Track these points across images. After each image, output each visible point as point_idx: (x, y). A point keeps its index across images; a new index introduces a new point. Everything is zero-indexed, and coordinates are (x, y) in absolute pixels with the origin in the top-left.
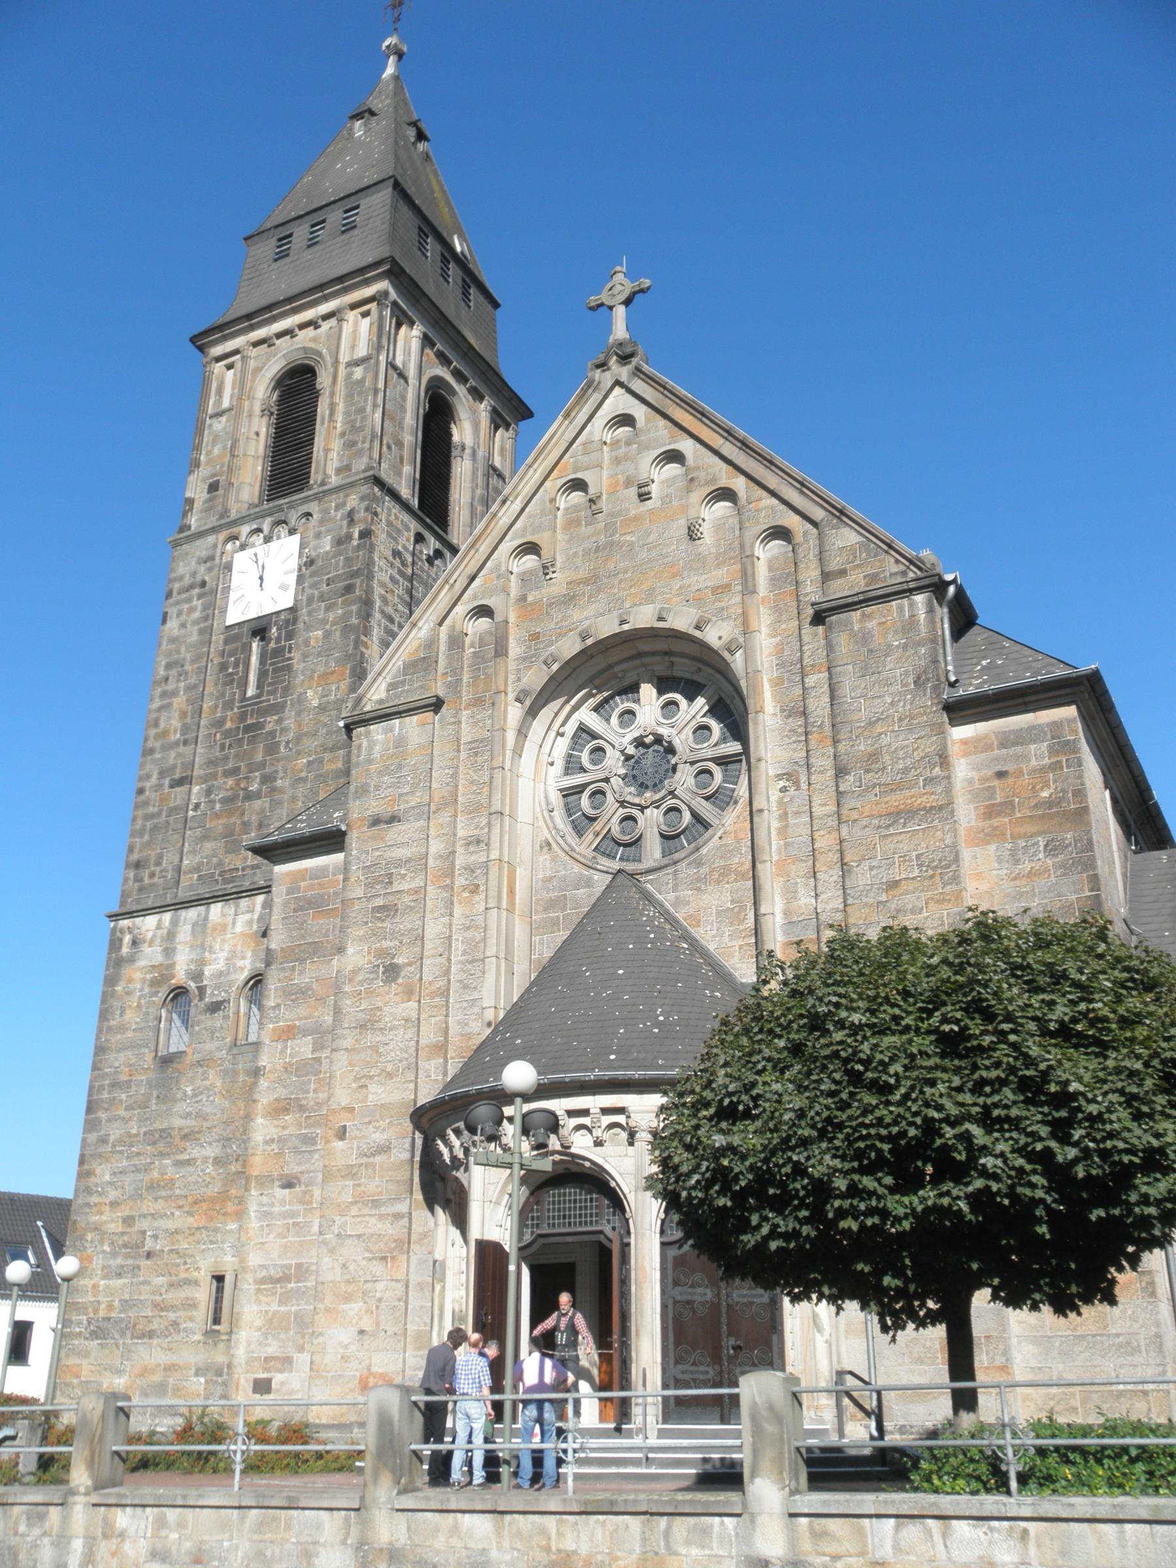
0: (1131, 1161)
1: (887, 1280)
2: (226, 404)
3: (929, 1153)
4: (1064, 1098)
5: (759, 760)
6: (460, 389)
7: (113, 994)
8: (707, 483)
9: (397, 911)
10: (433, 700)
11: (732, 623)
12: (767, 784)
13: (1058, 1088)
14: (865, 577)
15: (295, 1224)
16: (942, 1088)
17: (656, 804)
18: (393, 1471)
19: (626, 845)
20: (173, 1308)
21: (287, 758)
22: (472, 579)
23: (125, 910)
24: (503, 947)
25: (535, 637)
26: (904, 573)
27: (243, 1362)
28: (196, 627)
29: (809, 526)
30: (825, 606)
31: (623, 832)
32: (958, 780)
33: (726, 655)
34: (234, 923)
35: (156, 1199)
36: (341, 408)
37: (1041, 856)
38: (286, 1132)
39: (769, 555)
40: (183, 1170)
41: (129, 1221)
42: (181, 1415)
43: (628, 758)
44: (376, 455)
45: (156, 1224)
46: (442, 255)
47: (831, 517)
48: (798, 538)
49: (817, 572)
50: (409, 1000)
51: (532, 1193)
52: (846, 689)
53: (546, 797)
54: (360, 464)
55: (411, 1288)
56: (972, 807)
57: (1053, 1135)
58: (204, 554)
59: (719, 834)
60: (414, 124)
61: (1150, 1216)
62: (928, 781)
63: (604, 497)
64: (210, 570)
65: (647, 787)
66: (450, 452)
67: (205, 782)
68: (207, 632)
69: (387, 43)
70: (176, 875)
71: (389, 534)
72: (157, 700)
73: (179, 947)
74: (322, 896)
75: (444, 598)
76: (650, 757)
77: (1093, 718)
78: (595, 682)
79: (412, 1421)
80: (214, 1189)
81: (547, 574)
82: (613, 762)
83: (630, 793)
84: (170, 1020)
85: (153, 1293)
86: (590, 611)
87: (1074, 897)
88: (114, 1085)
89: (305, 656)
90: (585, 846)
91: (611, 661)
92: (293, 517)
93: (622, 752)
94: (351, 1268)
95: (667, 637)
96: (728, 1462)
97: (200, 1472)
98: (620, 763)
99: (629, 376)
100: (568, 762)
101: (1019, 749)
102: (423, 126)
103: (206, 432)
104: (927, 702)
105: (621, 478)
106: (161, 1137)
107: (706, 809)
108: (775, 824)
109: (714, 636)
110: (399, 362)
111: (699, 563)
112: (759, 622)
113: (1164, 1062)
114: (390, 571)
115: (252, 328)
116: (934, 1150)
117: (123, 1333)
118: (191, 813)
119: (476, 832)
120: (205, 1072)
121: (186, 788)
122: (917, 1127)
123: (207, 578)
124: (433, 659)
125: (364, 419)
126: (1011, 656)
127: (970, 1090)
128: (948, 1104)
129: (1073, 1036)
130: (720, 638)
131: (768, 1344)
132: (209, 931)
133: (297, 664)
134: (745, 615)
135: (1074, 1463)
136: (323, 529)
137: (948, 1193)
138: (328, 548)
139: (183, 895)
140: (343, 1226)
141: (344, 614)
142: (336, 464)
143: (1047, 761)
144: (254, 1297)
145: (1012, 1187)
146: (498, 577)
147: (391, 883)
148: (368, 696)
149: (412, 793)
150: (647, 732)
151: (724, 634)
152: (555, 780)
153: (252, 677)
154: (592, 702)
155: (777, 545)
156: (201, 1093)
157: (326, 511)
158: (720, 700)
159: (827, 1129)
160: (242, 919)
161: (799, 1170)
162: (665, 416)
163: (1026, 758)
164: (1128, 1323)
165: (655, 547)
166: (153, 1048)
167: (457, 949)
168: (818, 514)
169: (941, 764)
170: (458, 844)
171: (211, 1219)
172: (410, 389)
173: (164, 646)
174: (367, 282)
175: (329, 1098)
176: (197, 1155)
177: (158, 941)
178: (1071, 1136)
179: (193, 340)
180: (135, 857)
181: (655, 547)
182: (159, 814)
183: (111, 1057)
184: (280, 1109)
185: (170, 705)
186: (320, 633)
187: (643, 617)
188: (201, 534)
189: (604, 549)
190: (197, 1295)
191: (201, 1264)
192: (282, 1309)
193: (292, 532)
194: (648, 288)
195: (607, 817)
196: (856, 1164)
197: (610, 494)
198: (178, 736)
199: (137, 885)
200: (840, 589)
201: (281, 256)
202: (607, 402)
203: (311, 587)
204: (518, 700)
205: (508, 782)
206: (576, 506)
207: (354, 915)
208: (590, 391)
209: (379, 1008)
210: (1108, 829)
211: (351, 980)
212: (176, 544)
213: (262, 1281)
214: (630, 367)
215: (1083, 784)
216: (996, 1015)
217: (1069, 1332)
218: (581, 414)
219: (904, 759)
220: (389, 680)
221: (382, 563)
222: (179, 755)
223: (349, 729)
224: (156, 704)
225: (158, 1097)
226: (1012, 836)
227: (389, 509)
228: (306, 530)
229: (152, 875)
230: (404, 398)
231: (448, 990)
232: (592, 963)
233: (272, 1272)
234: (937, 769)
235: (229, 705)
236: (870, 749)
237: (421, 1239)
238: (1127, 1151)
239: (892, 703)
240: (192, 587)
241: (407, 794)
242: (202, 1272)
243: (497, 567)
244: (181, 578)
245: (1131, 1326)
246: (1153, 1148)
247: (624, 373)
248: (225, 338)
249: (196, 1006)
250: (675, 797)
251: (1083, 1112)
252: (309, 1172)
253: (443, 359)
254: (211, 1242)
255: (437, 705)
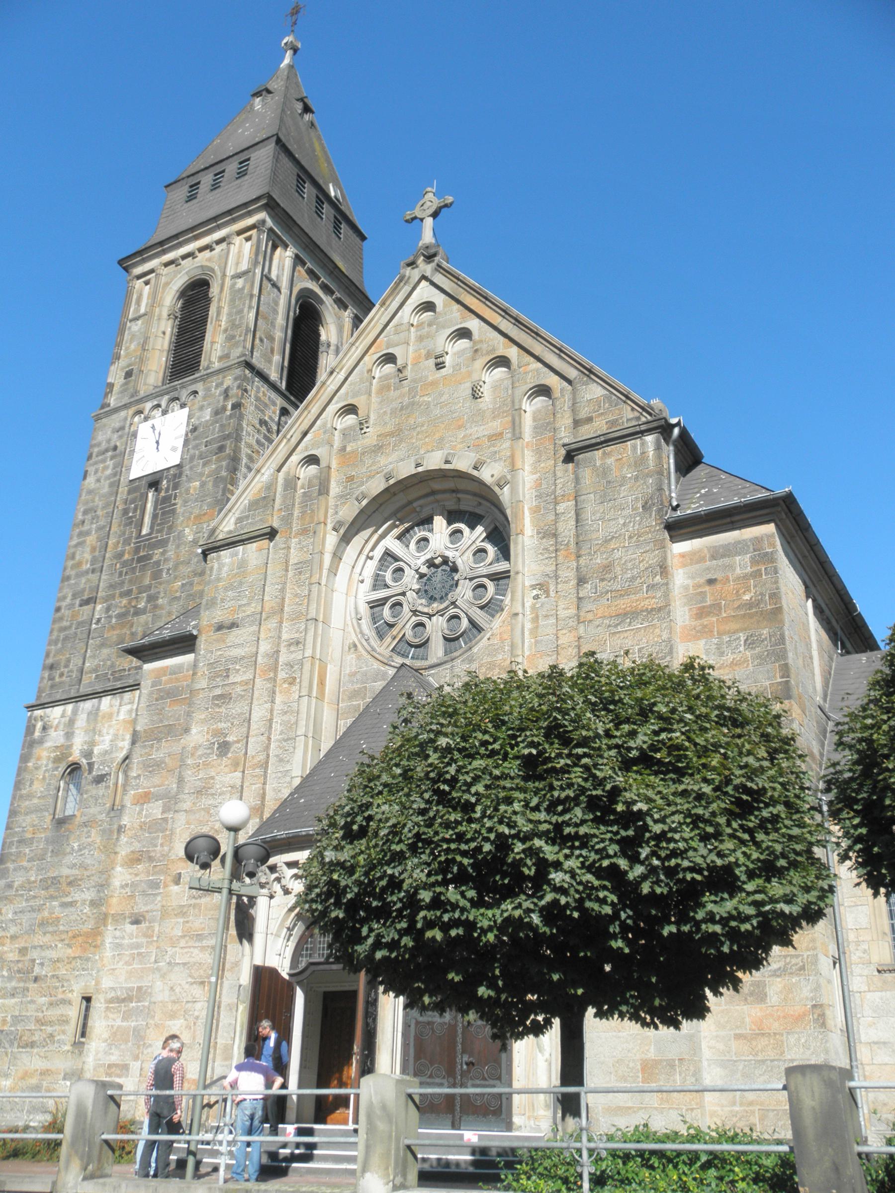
0: (693, 879)
1: (482, 991)
2: (142, 310)
3: (505, 868)
4: (631, 818)
5: (517, 573)
6: (328, 300)
7: (26, 769)
8: (488, 353)
9: (231, 698)
10: (268, 530)
11: (502, 463)
12: (523, 593)
13: (624, 808)
14: (607, 423)
15: (139, 954)
16: (517, 806)
17: (441, 613)
18: (81, 1159)
19: (417, 647)
20: (51, 1023)
21: (168, 582)
22: (305, 434)
23: (39, 702)
24: (311, 728)
25: (351, 479)
26: (638, 418)
27: (92, 1068)
28: (108, 482)
29: (565, 384)
30: (573, 446)
31: (415, 636)
32: (676, 587)
33: (496, 489)
34: (118, 712)
35: (45, 934)
36: (225, 310)
37: (742, 649)
38: (138, 878)
39: (533, 408)
40: (67, 910)
41: (23, 951)
42: (50, 1113)
43: (422, 576)
44: (249, 345)
45: (43, 954)
46: (317, 197)
47: (582, 376)
48: (556, 394)
49: (570, 421)
50: (235, 771)
51: (308, 928)
52: (588, 515)
53: (356, 608)
54: (236, 352)
55: (222, 1008)
56: (686, 608)
57: (624, 854)
58: (117, 425)
59: (488, 636)
60: (302, 100)
61: (715, 934)
62: (651, 587)
63: (409, 367)
64: (121, 437)
65: (435, 599)
66: (317, 348)
67: (106, 601)
68: (116, 485)
69: (285, 41)
70: (79, 674)
71: (257, 407)
72: (75, 538)
73: (77, 731)
74: (177, 688)
75: (283, 449)
76: (439, 575)
77: (792, 537)
78: (399, 516)
79: (106, 1113)
80: (89, 926)
81: (362, 429)
82: (410, 579)
83: (421, 604)
84: (67, 790)
85: (37, 1010)
86: (394, 457)
87: (767, 683)
88: (21, 841)
89: (186, 502)
90: (384, 648)
91: (411, 497)
92: (184, 394)
93: (417, 571)
94: (177, 990)
95: (453, 477)
96: (443, 1162)
97: (48, 1160)
98: (415, 580)
99: (432, 271)
100: (376, 580)
101: (726, 560)
102: (310, 102)
103: (127, 332)
104: (653, 522)
105: (423, 352)
106: (52, 883)
107: (480, 616)
108: (528, 626)
109: (487, 475)
110: (273, 276)
111: (479, 416)
112: (523, 462)
113: (736, 788)
114: (256, 436)
115: (164, 252)
116: (509, 865)
117: (11, 1043)
118: (94, 626)
119: (296, 635)
120: (89, 832)
121: (91, 606)
122: (492, 843)
123: (118, 444)
124: (272, 498)
125: (242, 318)
126: (725, 485)
127: (546, 810)
128: (520, 820)
129: (653, 765)
130: (492, 476)
131: (498, 1062)
132: (99, 718)
133: (180, 509)
134: (512, 457)
135: (652, 1168)
136: (205, 403)
137: (519, 906)
138: (208, 418)
139: (83, 690)
140: (173, 956)
141: (216, 469)
142: (219, 353)
143: (749, 570)
144: (103, 1014)
145: (581, 901)
146: (325, 432)
147: (228, 676)
148: (221, 528)
149: (249, 604)
150: (437, 555)
151: (495, 473)
152: (365, 594)
153: (147, 520)
154: (396, 532)
155: (540, 400)
156: (85, 848)
157: (208, 389)
158: (496, 528)
159: (418, 844)
160: (125, 709)
161: (395, 884)
162: (458, 301)
163: (731, 567)
164: (801, 1050)
165: (446, 405)
166: (51, 811)
167: (276, 730)
168: (572, 373)
169: (661, 573)
170: (282, 645)
171: (85, 950)
172: (282, 297)
173: (84, 497)
174: (250, 214)
175: (170, 850)
176: (78, 898)
177: (61, 727)
178: (639, 854)
179: (120, 262)
180: (50, 661)
181: (446, 405)
182: (70, 627)
183: (20, 818)
184: (135, 859)
185: (84, 542)
186: (198, 483)
187: (434, 461)
188: (116, 410)
189: (407, 408)
190: (70, 1013)
191: (74, 988)
192: (124, 1024)
193: (183, 406)
194: (451, 204)
195: (403, 623)
196: (440, 878)
197: (414, 365)
198: (88, 566)
199: (50, 682)
200: (587, 432)
201: (191, 198)
202: (415, 293)
203: (193, 448)
204: (334, 529)
205: (323, 595)
206: (387, 375)
207: (199, 702)
208: (402, 284)
209: (213, 778)
210: (807, 630)
211: (192, 755)
212: (98, 418)
213: (111, 1001)
214: (433, 265)
215: (778, 588)
216: (572, 739)
217: (751, 1057)
218: (394, 302)
219: (631, 569)
220: (237, 515)
221: (250, 429)
222: (88, 580)
223: (205, 554)
224: (74, 542)
225: (53, 851)
226: (718, 632)
227: (258, 388)
228: (193, 405)
229: (62, 675)
230: (276, 303)
231: (267, 763)
232: (368, 738)
233: (119, 993)
234: (658, 577)
235: (127, 542)
236: (605, 562)
237: (232, 968)
238: (691, 869)
239: (624, 524)
240: (107, 451)
241: (244, 605)
242: (75, 994)
243: (324, 425)
244: (99, 444)
245: (803, 1053)
246: (716, 866)
247: (427, 269)
248: (144, 261)
249: (86, 777)
250: (456, 607)
251: (650, 832)
252: (152, 911)
253: (312, 274)
254: (83, 969)
255: (272, 534)
